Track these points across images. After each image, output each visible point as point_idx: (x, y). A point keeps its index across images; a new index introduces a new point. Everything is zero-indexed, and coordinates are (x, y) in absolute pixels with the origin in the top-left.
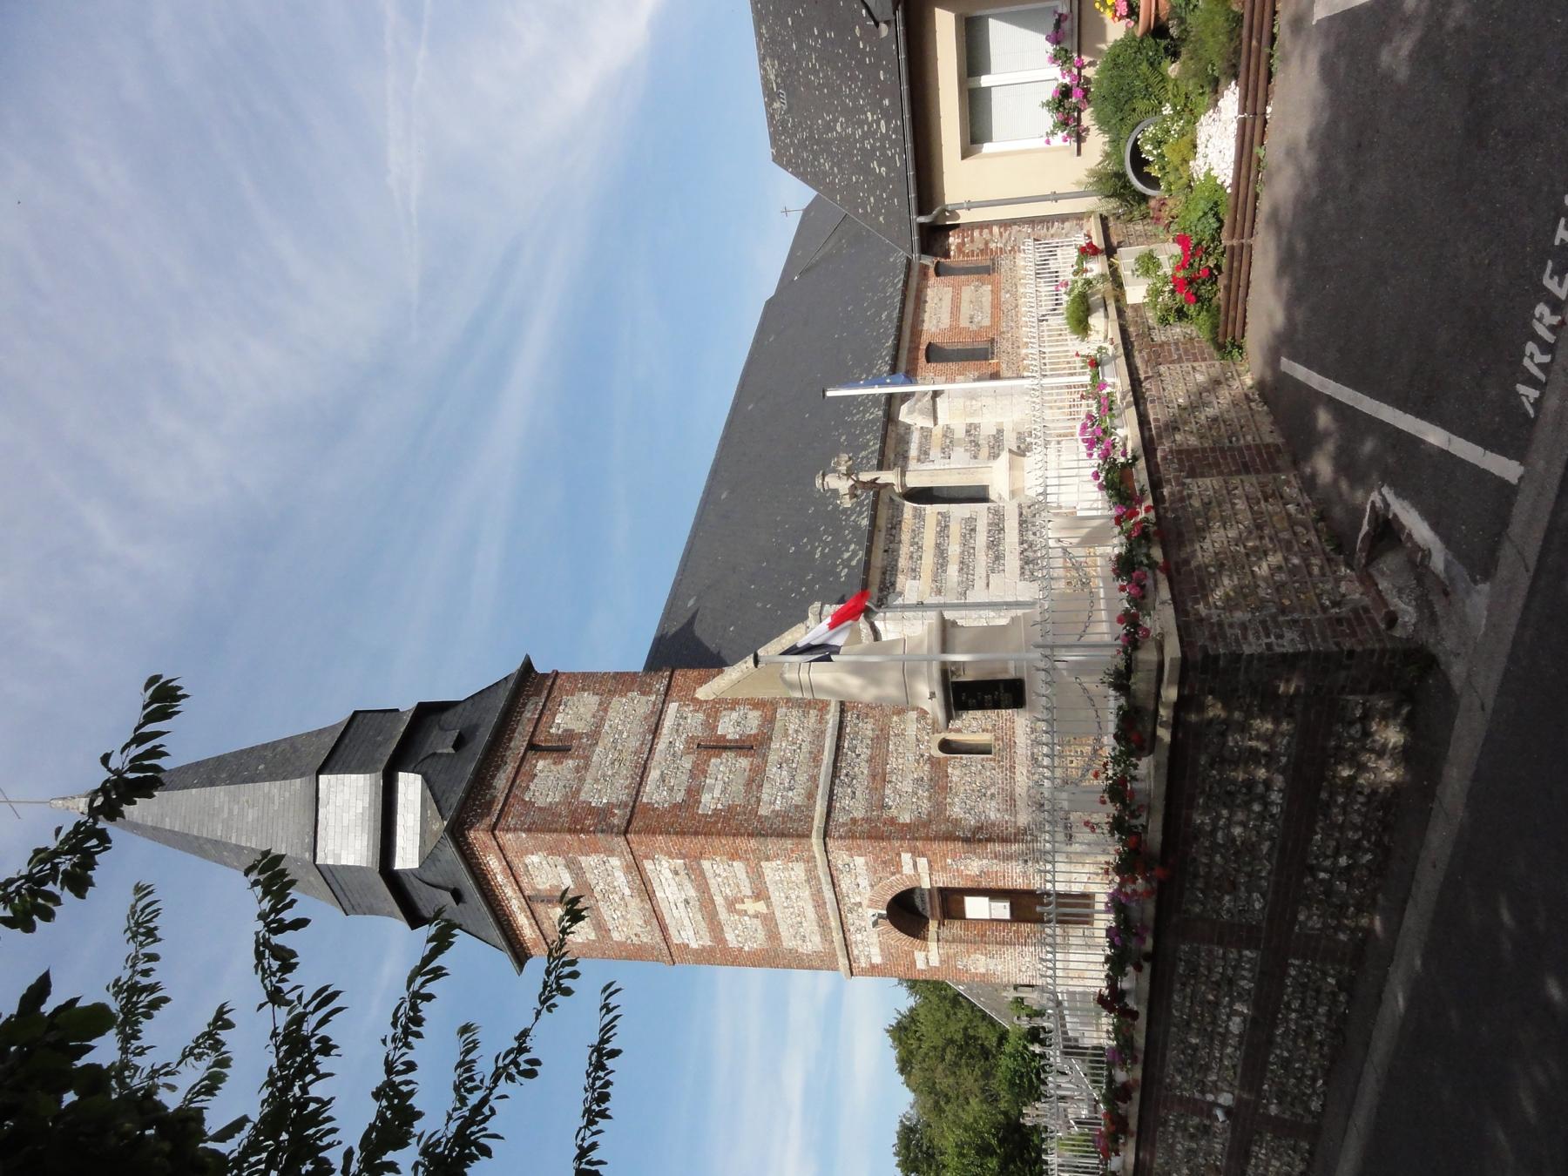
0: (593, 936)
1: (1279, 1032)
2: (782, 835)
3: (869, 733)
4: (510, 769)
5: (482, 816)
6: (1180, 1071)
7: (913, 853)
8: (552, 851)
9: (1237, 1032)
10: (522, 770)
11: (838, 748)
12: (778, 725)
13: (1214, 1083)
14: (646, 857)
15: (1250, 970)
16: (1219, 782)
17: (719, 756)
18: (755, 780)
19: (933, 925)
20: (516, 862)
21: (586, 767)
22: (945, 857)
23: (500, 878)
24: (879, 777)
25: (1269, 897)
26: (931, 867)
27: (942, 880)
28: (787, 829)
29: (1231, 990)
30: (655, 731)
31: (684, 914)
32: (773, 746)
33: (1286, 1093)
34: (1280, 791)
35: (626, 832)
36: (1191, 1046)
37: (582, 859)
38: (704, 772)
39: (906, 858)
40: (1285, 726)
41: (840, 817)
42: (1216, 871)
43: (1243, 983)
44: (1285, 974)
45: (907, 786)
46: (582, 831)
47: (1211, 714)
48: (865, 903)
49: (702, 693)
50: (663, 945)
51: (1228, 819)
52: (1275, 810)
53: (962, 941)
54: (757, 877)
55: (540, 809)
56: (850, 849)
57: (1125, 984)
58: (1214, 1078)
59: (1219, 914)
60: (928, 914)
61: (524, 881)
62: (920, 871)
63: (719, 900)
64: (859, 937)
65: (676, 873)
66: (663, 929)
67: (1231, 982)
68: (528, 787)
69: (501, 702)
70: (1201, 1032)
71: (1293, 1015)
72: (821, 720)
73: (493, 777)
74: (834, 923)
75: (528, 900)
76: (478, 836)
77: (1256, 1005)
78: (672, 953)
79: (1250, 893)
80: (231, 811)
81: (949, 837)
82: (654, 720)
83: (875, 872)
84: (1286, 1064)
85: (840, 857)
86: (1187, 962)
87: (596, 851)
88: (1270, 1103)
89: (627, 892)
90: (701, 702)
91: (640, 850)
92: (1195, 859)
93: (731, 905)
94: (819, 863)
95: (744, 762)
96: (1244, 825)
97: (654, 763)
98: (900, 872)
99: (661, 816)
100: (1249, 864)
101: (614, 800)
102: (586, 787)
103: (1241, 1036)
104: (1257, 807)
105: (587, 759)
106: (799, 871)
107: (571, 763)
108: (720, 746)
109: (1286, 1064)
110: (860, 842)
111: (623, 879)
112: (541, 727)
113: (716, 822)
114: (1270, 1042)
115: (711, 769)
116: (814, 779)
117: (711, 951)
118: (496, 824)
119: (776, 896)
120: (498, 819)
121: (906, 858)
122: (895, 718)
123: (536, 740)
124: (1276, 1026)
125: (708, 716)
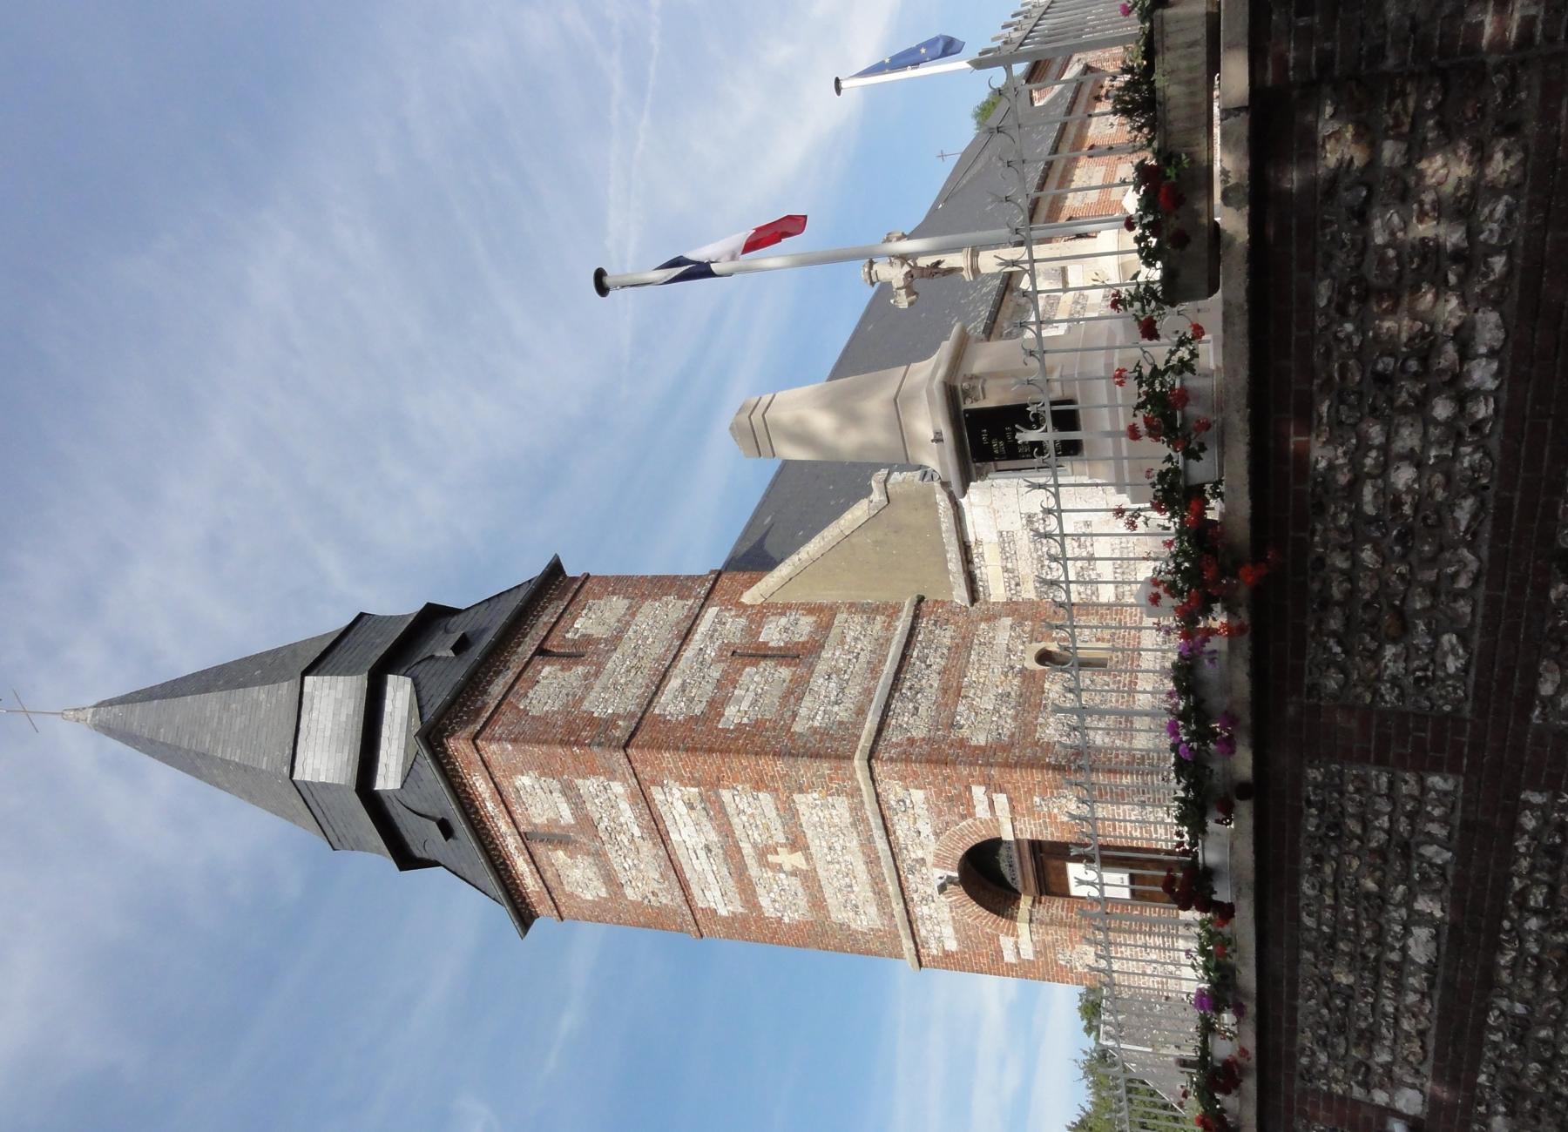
0: (603, 893)
1: (1505, 960)
2: (816, 756)
3: (947, 641)
4: (509, 676)
5: (467, 723)
6: (1323, 1042)
7: (988, 786)
8: (545, 770)
9: (1422, 960)
10: (525, 676)
11: (904, 656)
12: (835, 631)
13: (1388, 1067)
14: (654, 783)
15: (1444, 821)
16: (1359, 354)
17: (755, 665)
18: (795, 692)
19: (1025, 903)
20: (504, 784)
21: (596, 675)
22: (1030, 793)
23: (490, 806)
24: (953, 690)
25: (1476, 640)
26: (1013, 809)
27: (1030, 830)
28: (827, 749)
29: (1407, 868)
30: (686, 637)
31: (706, 867)
32: (825, 654)
33: (1522, 1093)
34: (1492, 354)
35: (626, 746)
36: (1338, 990)
37: (579, 782)
38: (734, 684)
39: (978, 792)
40: (1500, 166)
41: (893, 736)
42: (1367, 587)
43: (1429, 851)
44: (1514, 828)
45: (987, 703)
46: (576, 743)
47: (1332, 160)
48: (930, 859)
49: (748, 598)
50: (685, 908)
51: (1384, 449)
52: (1483, 410)
53: (1062, 924)
54: (789, 814)
55: (533, 717)
56: (902, 778)
57: (1210, 855)
58: (1385, 1057)
59: (1376, 693)
60: (1020, 887)
61: (518, 811)
62: (998, 815)
63: (747, 848)
64: (925, 910)
65: (691, 807)
66: (684, 886)
67: (1407, 850)
68: (526, 695)
69: (515, 602)
70: (1357, 961)
71: (1533, 923)
72: (889, 627)
73: (490, 683)
74: (892, 888)
75: (524, 837)
76: (458, 746)
77: (1457, 903)
78: (698, 921)
79: (1436, 636)
80: (220, 719)
81: (1033, 764)
82: (686, 625)
83: (940, 814)
84: (1520, 1030)
85: (893, 790)
86: (1323, 807)
87: (594, 772)
88: (1491, 1113)
89: (637, 832)
90: (745, 607)
91: (646, 773)
92: (1320, 562)
93: (762, 853)
94: (866, 798)
95: (785, 672)
96: (1418, 462)
97: (676, 671)
98: (972, 815)
99: (673, 729)
100: (1432, 561)
101: (621, 711)
102: (593, 695)
103: (1431, 968)
104: (1442, 409)
105: (600, 667)
106: (841, 809)
107: (580, 669)
108: (760, 654)
109: (1520, 1030)
110: (916, 767)
111: (629, 813)
112: (556, 632)
113: (737, 739)
114: (1489, 982)
115: (744, 679)
116: (868, 692)
117: (744, 919)
118: (479, 732)
119: (817, 845)
120: (483, 728)
121: (978, 792)
122: (983, 625)
123: (548, 646)
124: (1499, 947)
125: (752, 622)
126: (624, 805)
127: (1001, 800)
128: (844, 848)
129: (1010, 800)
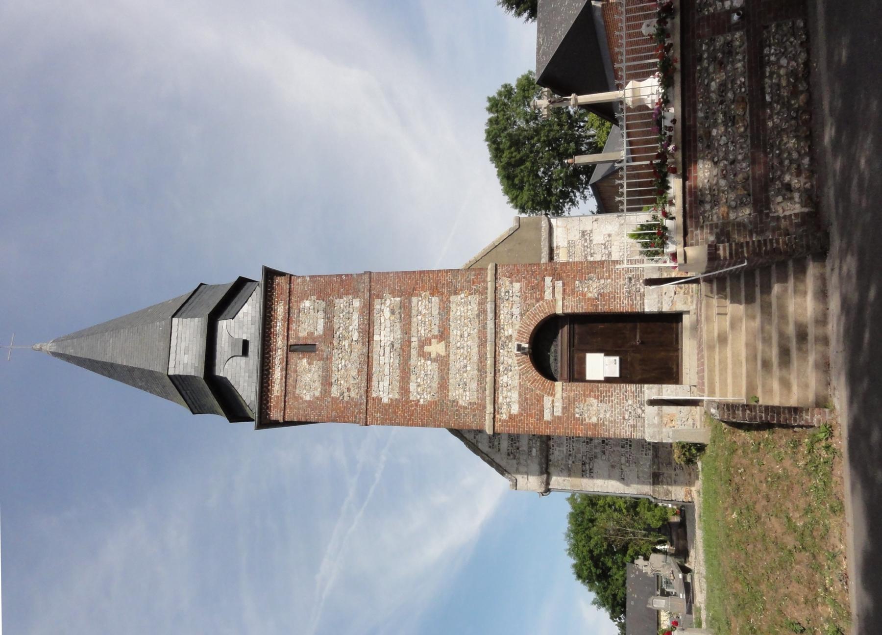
39: (548, 280)
61: (293, 326)
98: (542, 298)
126: (355, 316)
127: (559, 284)
128: (469, 335)
129: (564, 284)
